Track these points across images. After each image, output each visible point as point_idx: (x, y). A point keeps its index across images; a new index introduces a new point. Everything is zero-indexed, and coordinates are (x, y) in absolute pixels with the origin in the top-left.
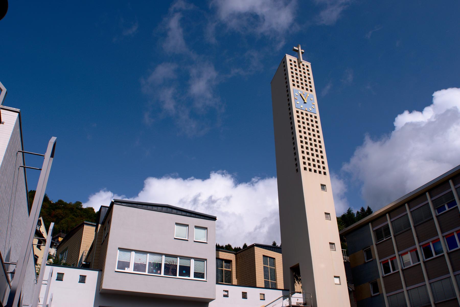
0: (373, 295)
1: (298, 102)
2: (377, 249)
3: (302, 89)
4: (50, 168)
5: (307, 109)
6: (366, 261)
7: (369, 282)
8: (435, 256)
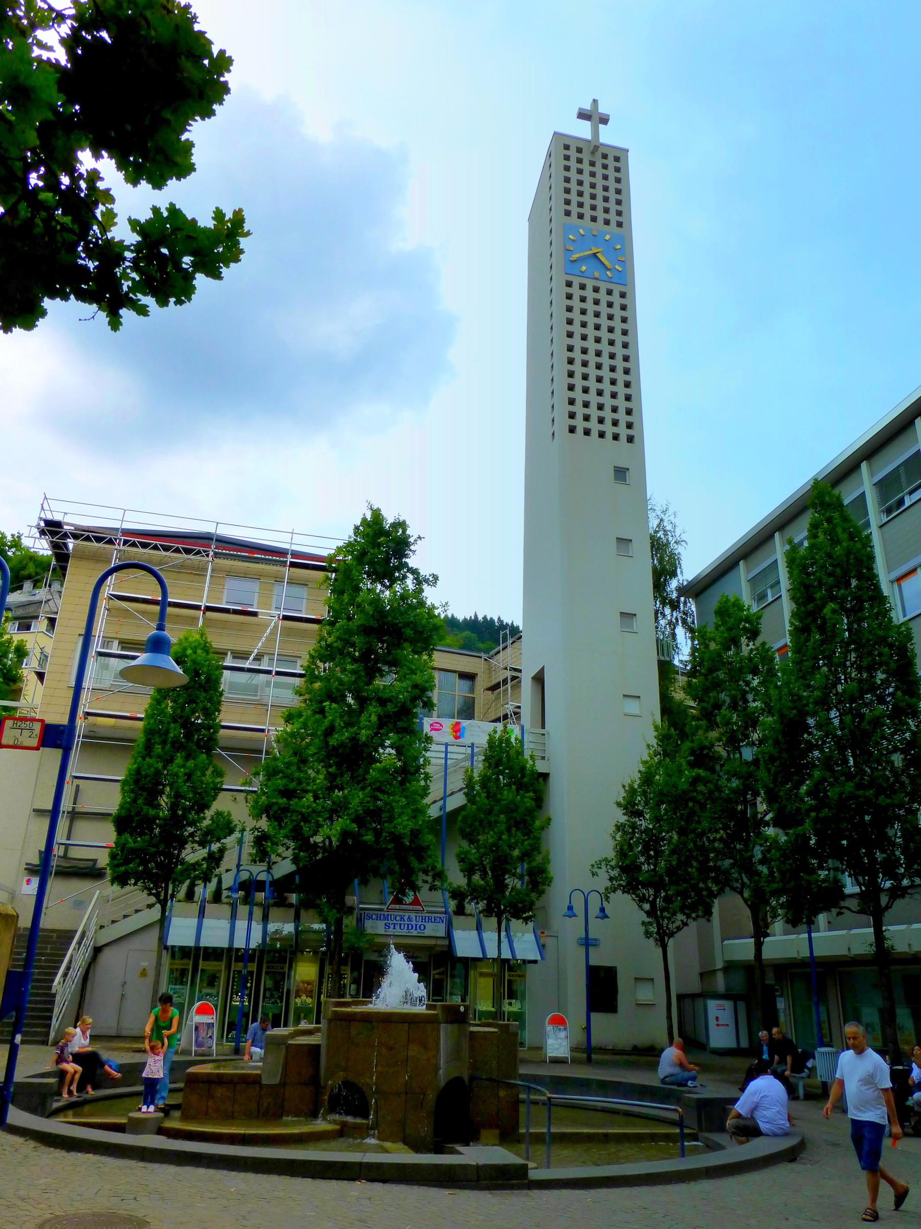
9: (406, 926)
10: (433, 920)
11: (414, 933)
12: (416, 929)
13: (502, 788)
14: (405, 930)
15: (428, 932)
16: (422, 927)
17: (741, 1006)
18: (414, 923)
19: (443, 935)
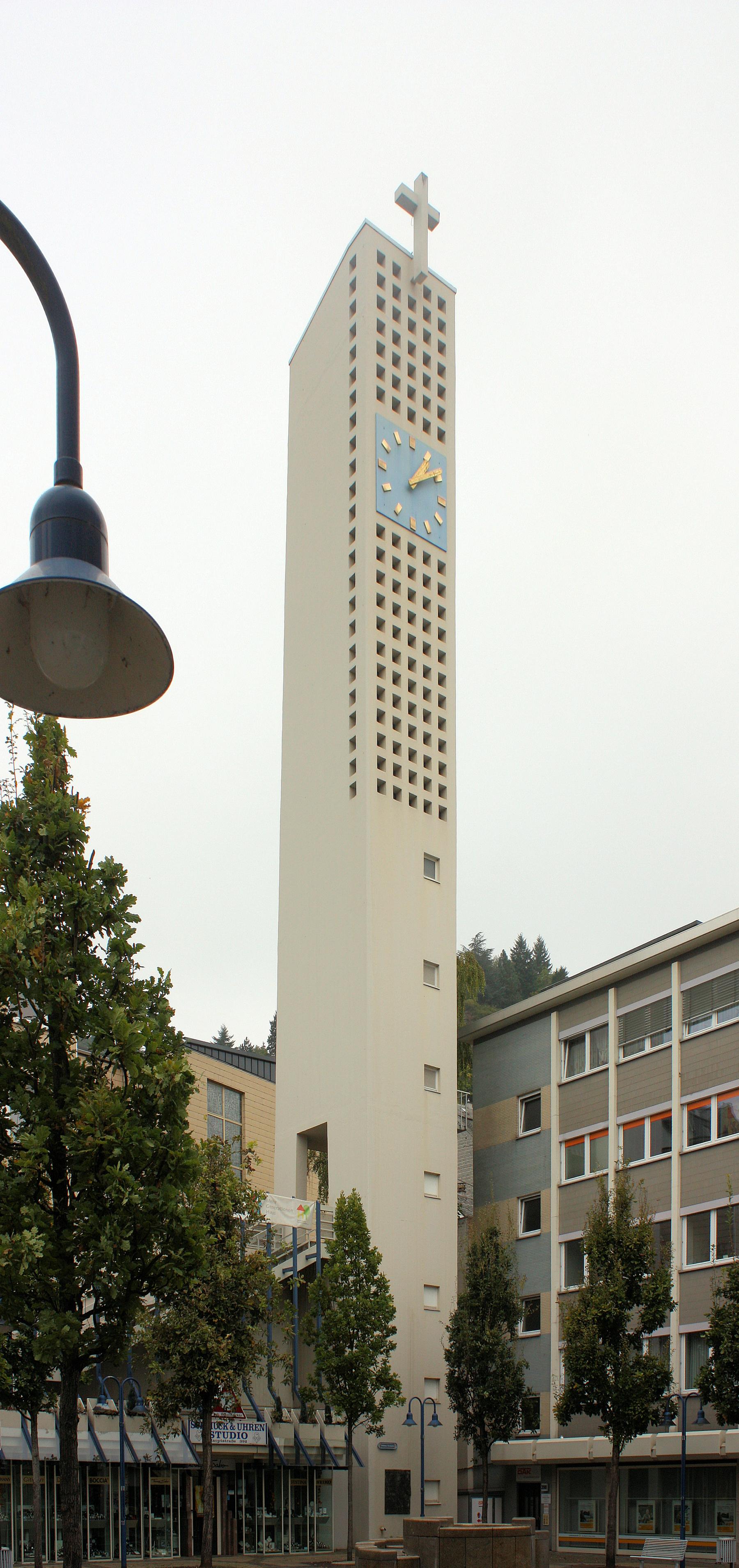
0: (522, 1234)
1: (388, 487)
2: (561, 1100)
3: (424, 432)
4: (371, 1510)
5: (414, 525)
6: (521, 1134)
7: (518, 1198)
8: (714, 1140)
9: (229, 1434)
10: (254, 1427)
11: (238, 1442)
12: (239, 1438)
13: (658, 1399)
14: (228, 1439)
15: (250, 1441)
16: (244, 1435)
17: (498, 1501)
18: (236, 1431)
19: (265, 1444)
